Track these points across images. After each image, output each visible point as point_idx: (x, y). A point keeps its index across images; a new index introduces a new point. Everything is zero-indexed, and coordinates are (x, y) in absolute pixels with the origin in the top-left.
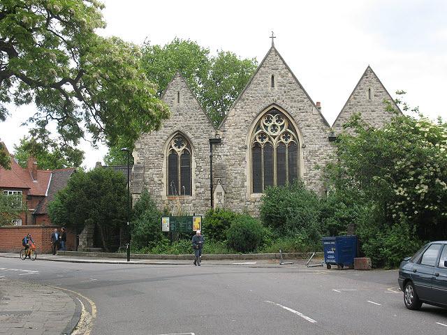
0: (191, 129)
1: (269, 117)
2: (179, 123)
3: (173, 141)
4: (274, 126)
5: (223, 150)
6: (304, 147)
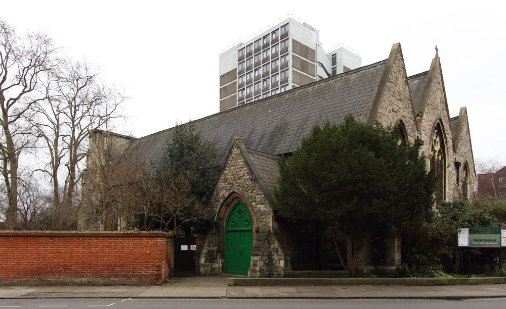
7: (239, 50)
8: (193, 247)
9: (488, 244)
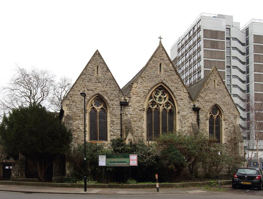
0: (107, 94)
1: (157, 91)
2: (98, 88)
3: (93, 102)
4: (160, 97)
5: (129, 110)
6: (178, 113)
7: (178, 45)
8: (11, 167)
9: (120, 164)
